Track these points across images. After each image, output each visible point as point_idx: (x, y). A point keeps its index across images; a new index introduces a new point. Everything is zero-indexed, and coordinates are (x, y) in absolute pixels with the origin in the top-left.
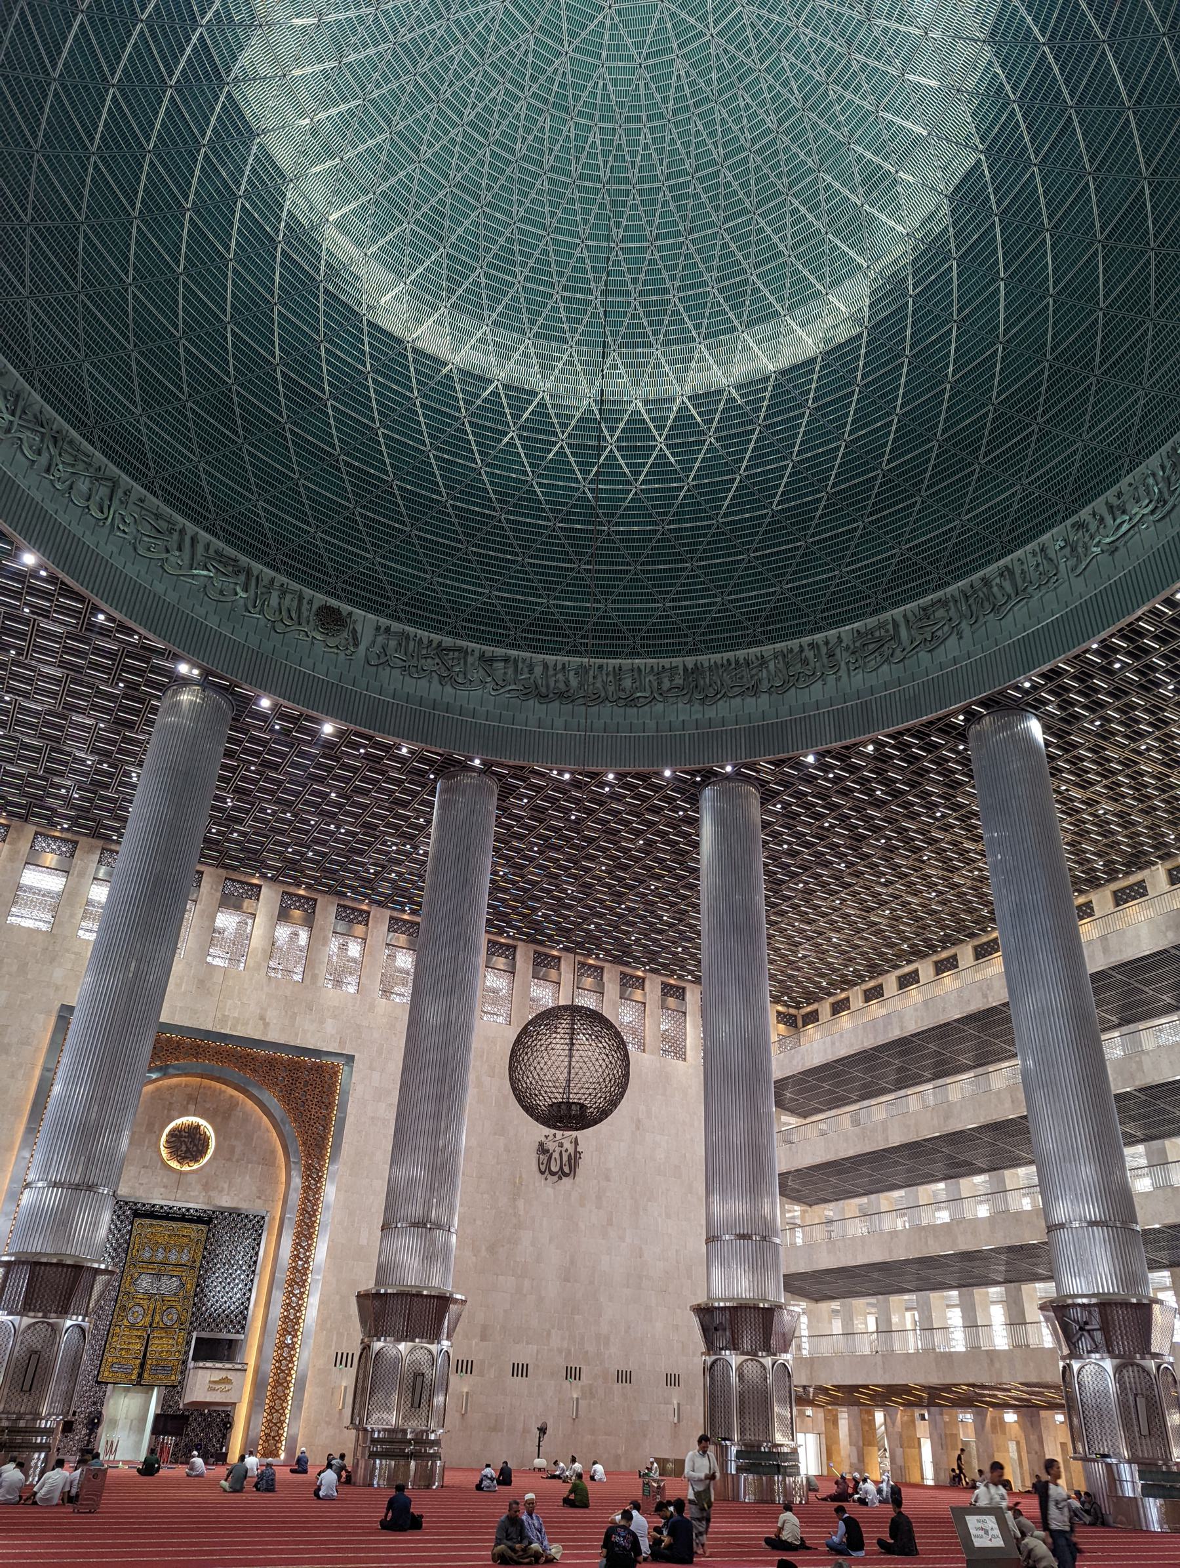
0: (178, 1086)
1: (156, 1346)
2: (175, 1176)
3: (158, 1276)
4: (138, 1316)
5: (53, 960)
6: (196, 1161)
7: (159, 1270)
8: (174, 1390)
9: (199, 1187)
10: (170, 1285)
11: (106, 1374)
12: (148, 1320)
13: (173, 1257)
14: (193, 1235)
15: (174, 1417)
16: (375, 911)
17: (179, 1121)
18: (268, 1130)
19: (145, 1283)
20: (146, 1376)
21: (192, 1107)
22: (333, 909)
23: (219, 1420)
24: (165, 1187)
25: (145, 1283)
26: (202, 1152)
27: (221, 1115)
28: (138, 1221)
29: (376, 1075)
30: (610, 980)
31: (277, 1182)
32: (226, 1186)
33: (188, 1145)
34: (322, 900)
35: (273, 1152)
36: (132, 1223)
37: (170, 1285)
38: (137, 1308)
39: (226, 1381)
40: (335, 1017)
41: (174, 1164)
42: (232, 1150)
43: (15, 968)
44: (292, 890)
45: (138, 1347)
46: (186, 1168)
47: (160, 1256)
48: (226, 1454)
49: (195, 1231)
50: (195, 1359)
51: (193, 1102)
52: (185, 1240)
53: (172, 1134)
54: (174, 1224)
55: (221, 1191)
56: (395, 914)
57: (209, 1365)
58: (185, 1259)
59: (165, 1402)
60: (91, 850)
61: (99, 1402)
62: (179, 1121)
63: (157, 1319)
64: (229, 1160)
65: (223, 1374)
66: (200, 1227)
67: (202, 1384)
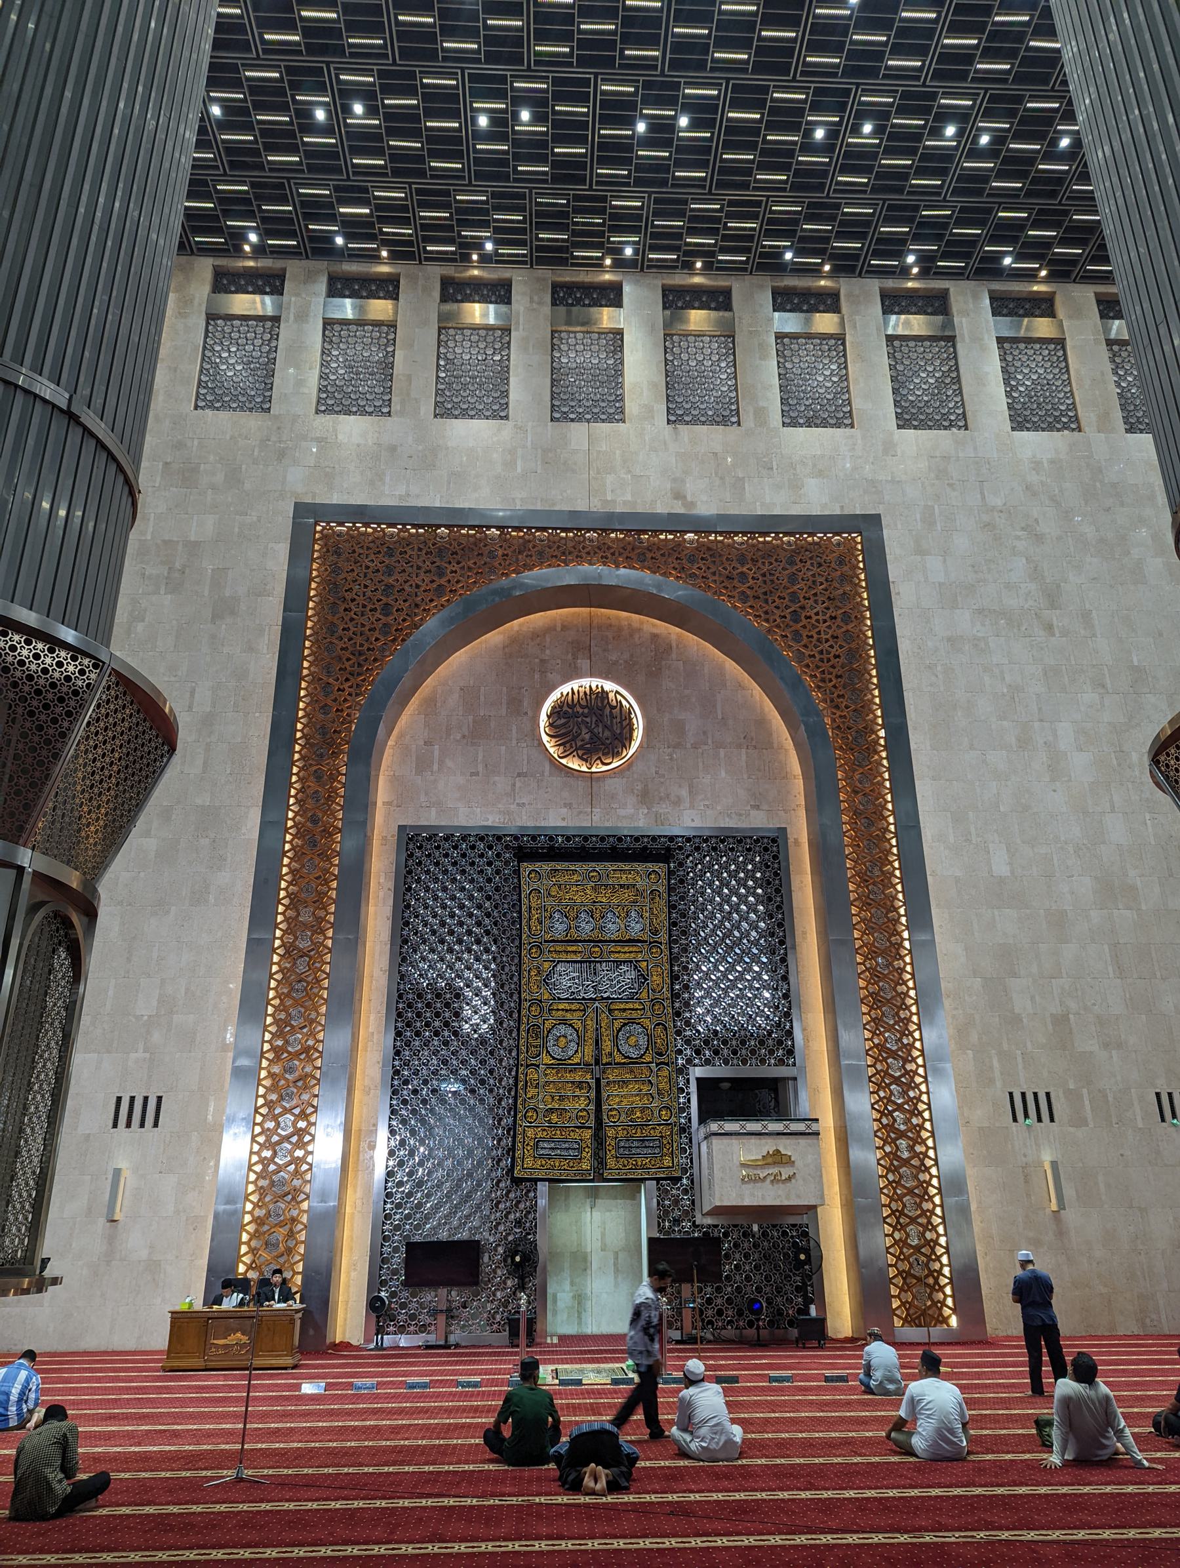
0: (550, 629)
1: (618, 1099)
2: (581, 785)
3: (589, 963)
4: (563, 1043)
5: (281, 454)
6: (616, 754)
7: (593, 952)
8: (677, 1183)
9: (631, 800)
10: (617, 981)
11: (528, 1165)
12: (589, 1052)
13: (612, 928)
14: (641, 883)
15: (685, 1243)
16: (846, 287)
17: (566, 689)
18: (741, 686)
19: (567, 979)
20: (611, 1162)
21: (584, 663)
22: (767, 298)
23: (786, 1243)
24: (569, 806)
25: (567, 979)
26: (624, 738)
27: (646, 668)
28: (527, 867)
29: (934, 563)
30: (466, 652)
31: (786, 776)
32: (684, 793)
33: (591, 728)
34: (738, 287)
35: (762, 723)
36: (517, 872)
37: (617, 981)
38: (563, 1029)
39: (777, 1159)
40: (820, 474)
41: (574, 764)
42: (679, 728)
43: (219, 478)
44: (680, 279)
45: (581, 1103)
46: (598, 768)
47: (586, 927)
48: (821, 1322)
49: (641, 876)
50: (702, 1120)
51: (583, 651)
52: (627, 895)
53: (556, 712)
54: (599, 867)
55: (678, 802)
56: (890, 283)
57: (730, 1126)
58: (636, 928)
59: (662, 1214)
60: (310, 277)
61: (527, 1223)
62: (566, 689)
63: (607, 1045)
64: (678, 746)
65: (769, 1146)
66: (651, 866)
67: (732, 1168)
